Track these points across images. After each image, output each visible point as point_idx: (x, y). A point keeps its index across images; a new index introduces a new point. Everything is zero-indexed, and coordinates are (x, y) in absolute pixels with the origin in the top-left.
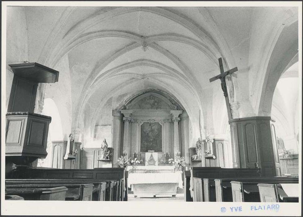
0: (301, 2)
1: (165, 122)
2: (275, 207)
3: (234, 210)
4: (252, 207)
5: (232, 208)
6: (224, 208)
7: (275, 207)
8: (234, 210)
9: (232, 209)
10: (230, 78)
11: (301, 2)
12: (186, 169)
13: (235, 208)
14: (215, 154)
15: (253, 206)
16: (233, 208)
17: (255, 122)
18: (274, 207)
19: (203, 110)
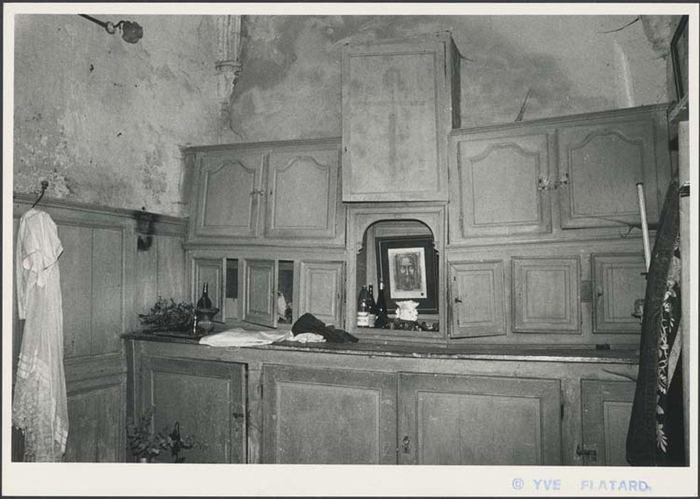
0: (5, 493)
1: (365, 419)
2: (637, 488)
3: (542, 484)
4: (586, 484)
5: (538, 481)
6: (522, 488)
7: (637, 488)
8: (542, 484)
9: (538, 484)
10: (43, 387)
11: (5, 493)
12: (587, 307)
13: (545, 482)
14: (529, 123)
15: (588, 482)
16: (541, 480)
17: (131, 223)
18: (635, 487)
19: (619, 129)
